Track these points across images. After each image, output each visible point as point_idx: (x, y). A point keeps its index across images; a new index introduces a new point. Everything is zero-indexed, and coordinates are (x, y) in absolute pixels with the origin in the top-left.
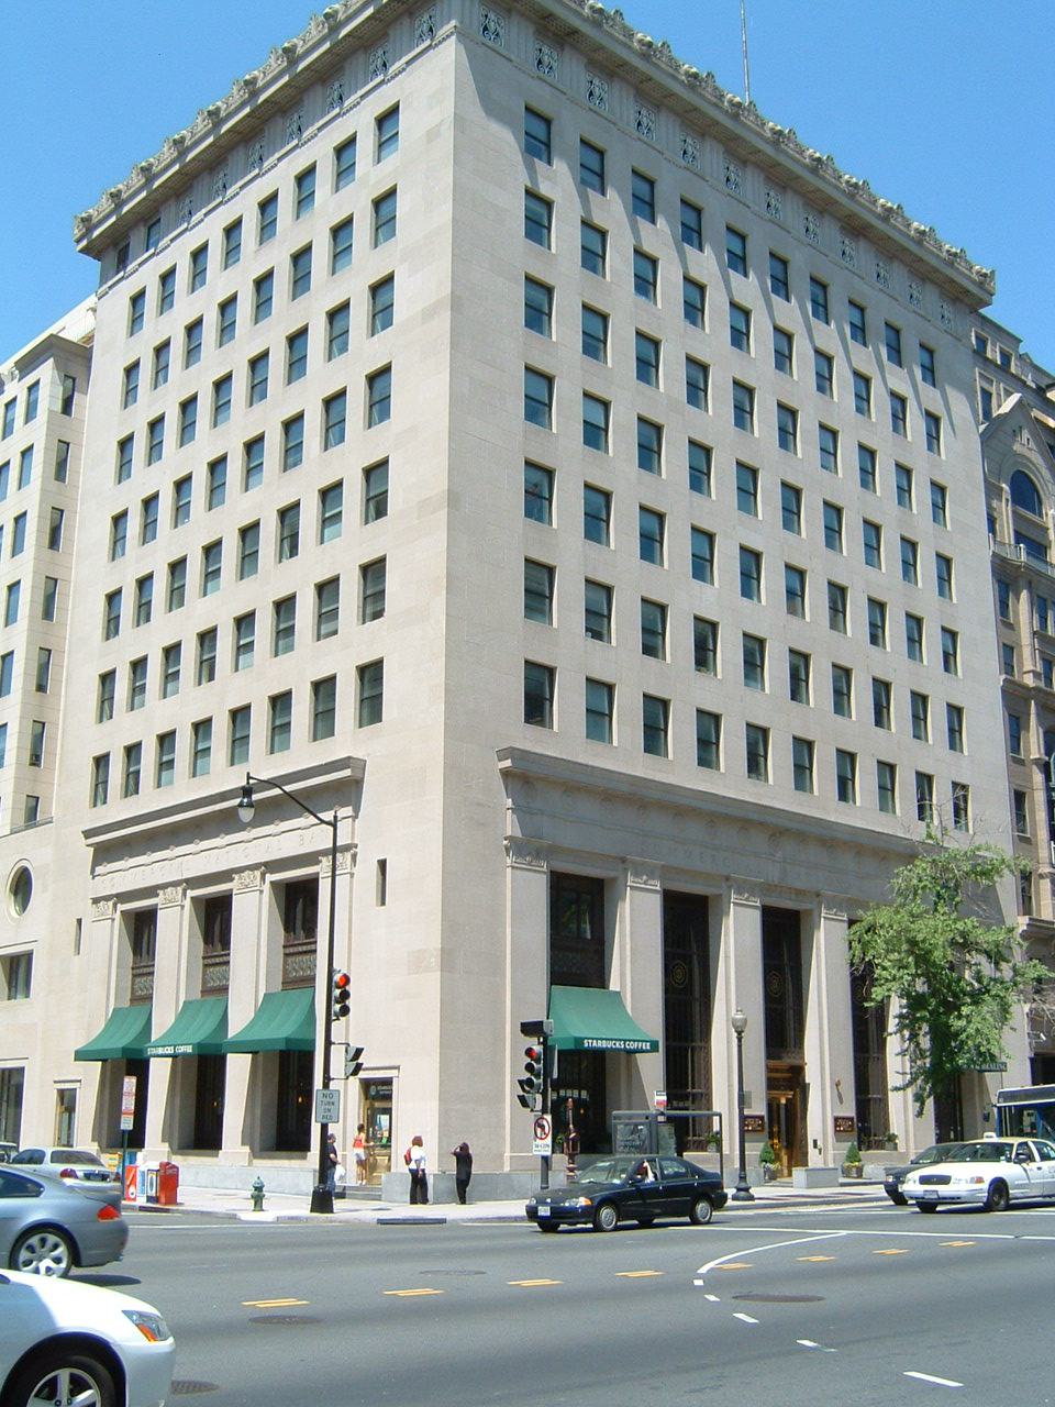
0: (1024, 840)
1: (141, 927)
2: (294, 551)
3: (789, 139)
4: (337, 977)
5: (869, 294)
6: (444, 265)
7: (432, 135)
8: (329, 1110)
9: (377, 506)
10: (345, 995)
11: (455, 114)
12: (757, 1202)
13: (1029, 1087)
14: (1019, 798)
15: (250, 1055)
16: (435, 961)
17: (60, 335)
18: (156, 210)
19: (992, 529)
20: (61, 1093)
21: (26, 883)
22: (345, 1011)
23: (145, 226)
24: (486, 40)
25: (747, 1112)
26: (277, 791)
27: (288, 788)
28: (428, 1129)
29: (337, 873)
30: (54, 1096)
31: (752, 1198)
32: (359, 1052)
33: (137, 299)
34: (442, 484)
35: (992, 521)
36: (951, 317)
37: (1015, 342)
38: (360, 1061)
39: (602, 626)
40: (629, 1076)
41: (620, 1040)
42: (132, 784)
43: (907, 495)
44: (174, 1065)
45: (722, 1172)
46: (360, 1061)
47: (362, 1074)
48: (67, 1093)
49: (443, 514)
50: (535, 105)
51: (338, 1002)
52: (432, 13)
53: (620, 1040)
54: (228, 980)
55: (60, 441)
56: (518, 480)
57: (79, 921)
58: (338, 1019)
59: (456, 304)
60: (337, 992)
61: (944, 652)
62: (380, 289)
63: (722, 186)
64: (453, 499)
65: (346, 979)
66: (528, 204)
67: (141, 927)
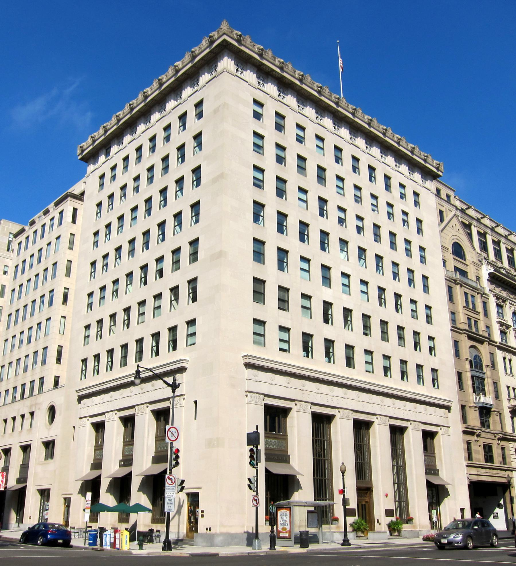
0: (479, 385)
1: (99, 427)
4: (174, 450)
8: (170, 507)
9: (194, 256)
10: (177, 457)
12: (352, 546)
13: (503, 509)
14: (460, 375)
17: (72, 192)
19: (444, 265)
22: (177, 464)
24: (237, 74)
25: (347, 507)
26: (151, 373)
27: (156, 372)
29: (175, 407)
31: (350, 545)
32: (183, 481)
33: (102, 177)
35: (444, 262)
38: (183, 485)
39: (285, 307)
40: (433, 443)
42: (97, 370)
43: (386, 335)
45: (398, 271)
46: (183, 485)
47: (185, 491)
50: (257, 99)
51: (174, 460)
54: (133, 452)
55: (71, 234)
56: (250, 247)
58: (174, 468)
60: (174, 456)
61: (414, 342)
62: (197, 171)
65: (178, 450)
67: (99, 427)
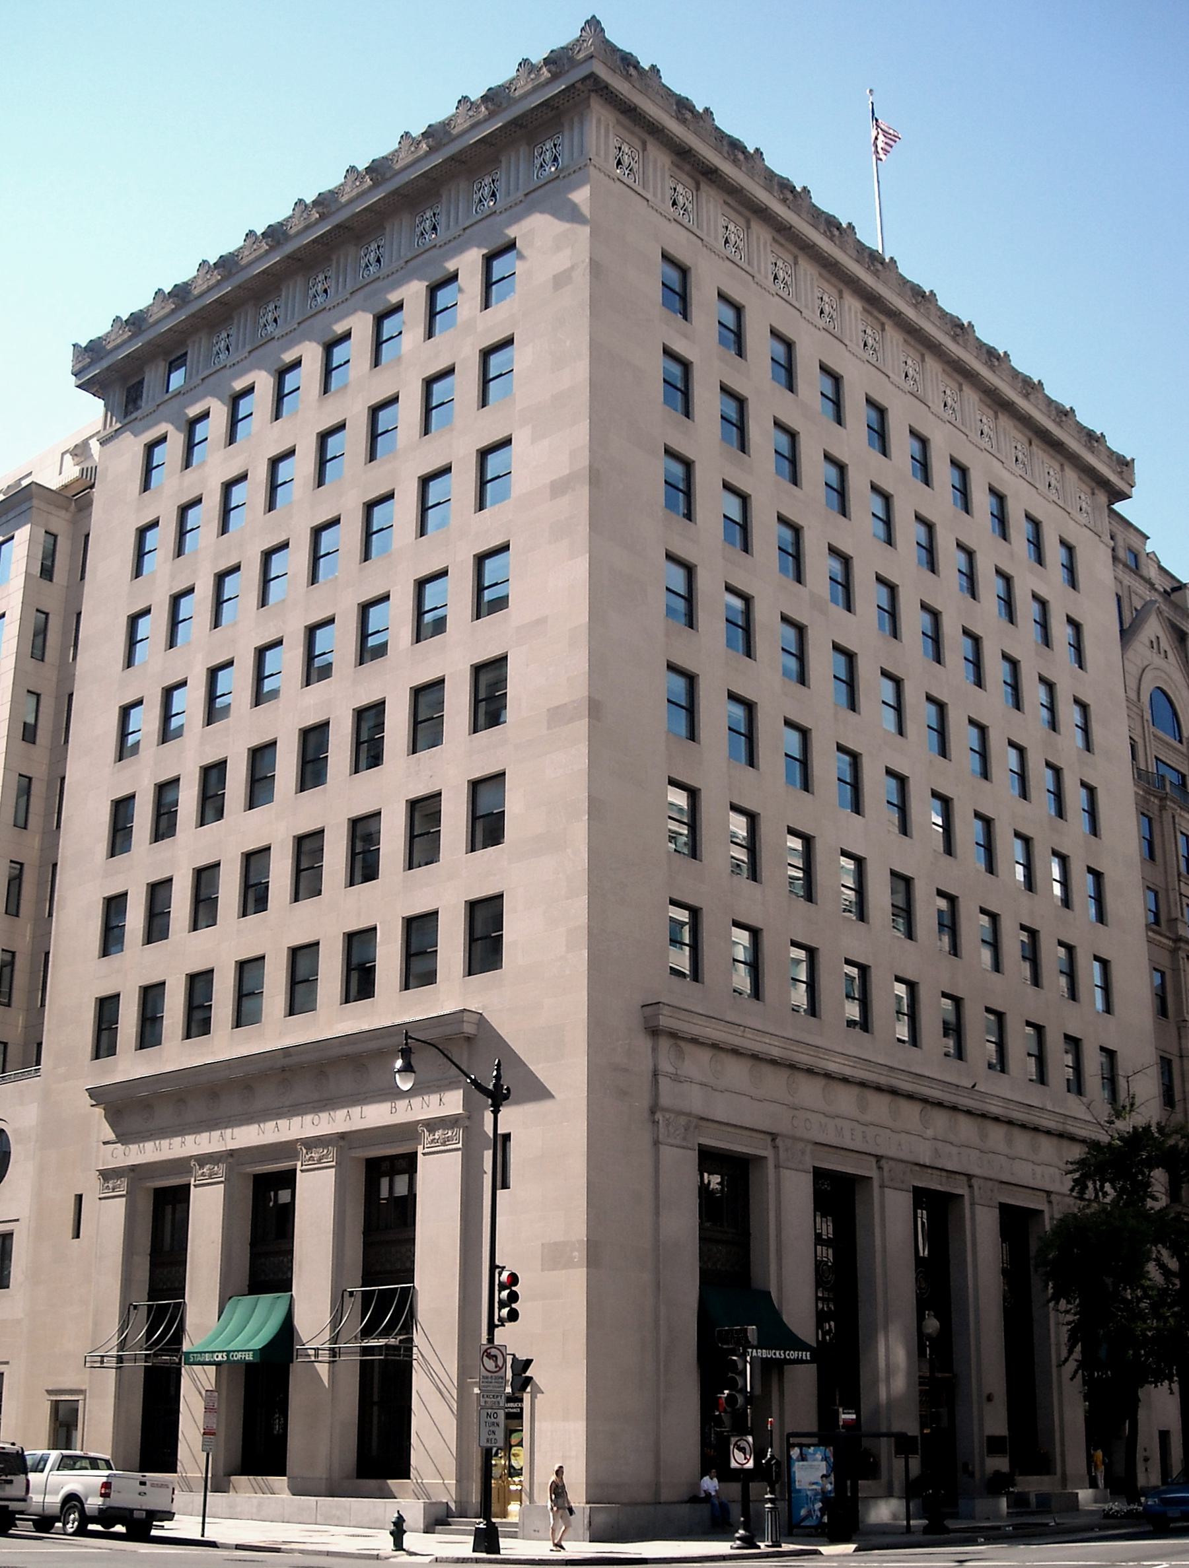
2: (375, 760)
3: (930, 301)
5: (1011, 485)
6: (581, 433)
7: (560, 281)
8: (494, 1433)
11: (591, 259)
15: (214, 1367)
16: (579, 1255)
18: (182, 343)
20: (56, 1405)
21: (231, 1155)
23: (165, 360)
28: (573, 1454)
30: (46, 1409)
34: (581, 691)
36: (1089, 509)
37: (1142, 538)
38: (528, 1374)
41: (223, 1352)
44: (218, 1374)
46: (528, 1374)
48: (61, 1406)
49: (583, 725)
50: (673, 251)
52: (558, 142)
53: (223, 1352)
57: (79, 1198)
59: (595, 478)
63: (859, 350)
64: (595, 709)
65: (514, 1279)
66: (666, 366)
